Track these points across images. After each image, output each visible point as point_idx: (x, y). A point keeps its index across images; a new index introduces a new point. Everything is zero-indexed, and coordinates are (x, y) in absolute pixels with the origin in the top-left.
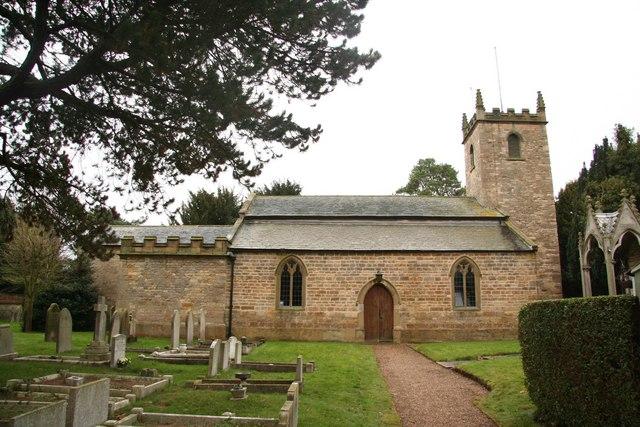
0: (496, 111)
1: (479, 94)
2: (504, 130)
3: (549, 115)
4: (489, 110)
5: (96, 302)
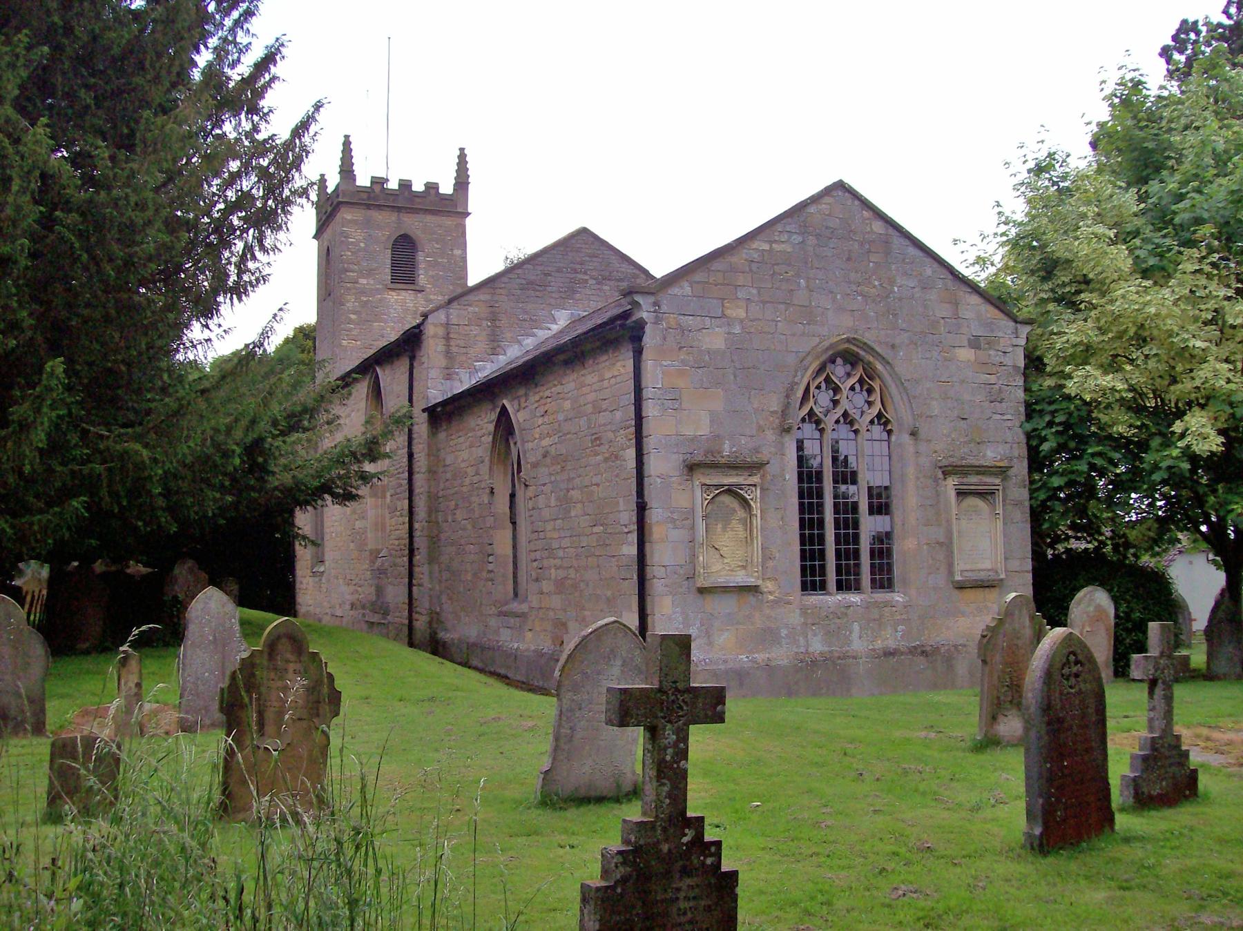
0: (378, 182)
1: (347, 144)
2: (387, 224)
3: (475, 199)
4: (363, 180)
5: (689, 877)
